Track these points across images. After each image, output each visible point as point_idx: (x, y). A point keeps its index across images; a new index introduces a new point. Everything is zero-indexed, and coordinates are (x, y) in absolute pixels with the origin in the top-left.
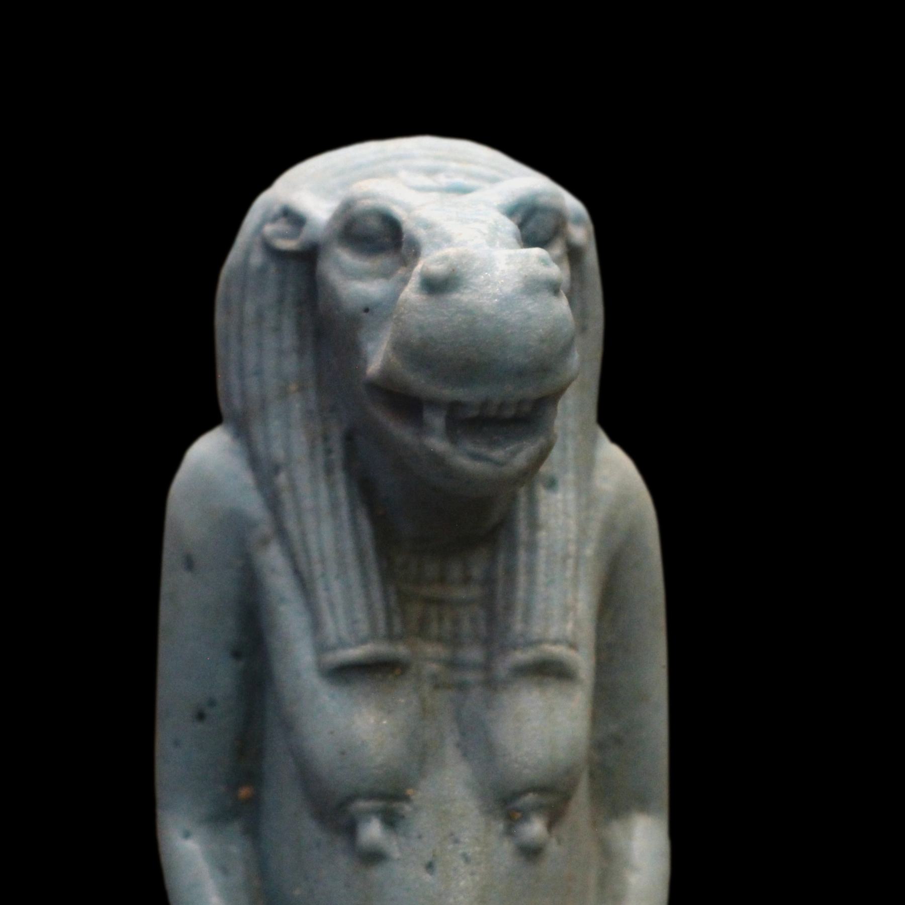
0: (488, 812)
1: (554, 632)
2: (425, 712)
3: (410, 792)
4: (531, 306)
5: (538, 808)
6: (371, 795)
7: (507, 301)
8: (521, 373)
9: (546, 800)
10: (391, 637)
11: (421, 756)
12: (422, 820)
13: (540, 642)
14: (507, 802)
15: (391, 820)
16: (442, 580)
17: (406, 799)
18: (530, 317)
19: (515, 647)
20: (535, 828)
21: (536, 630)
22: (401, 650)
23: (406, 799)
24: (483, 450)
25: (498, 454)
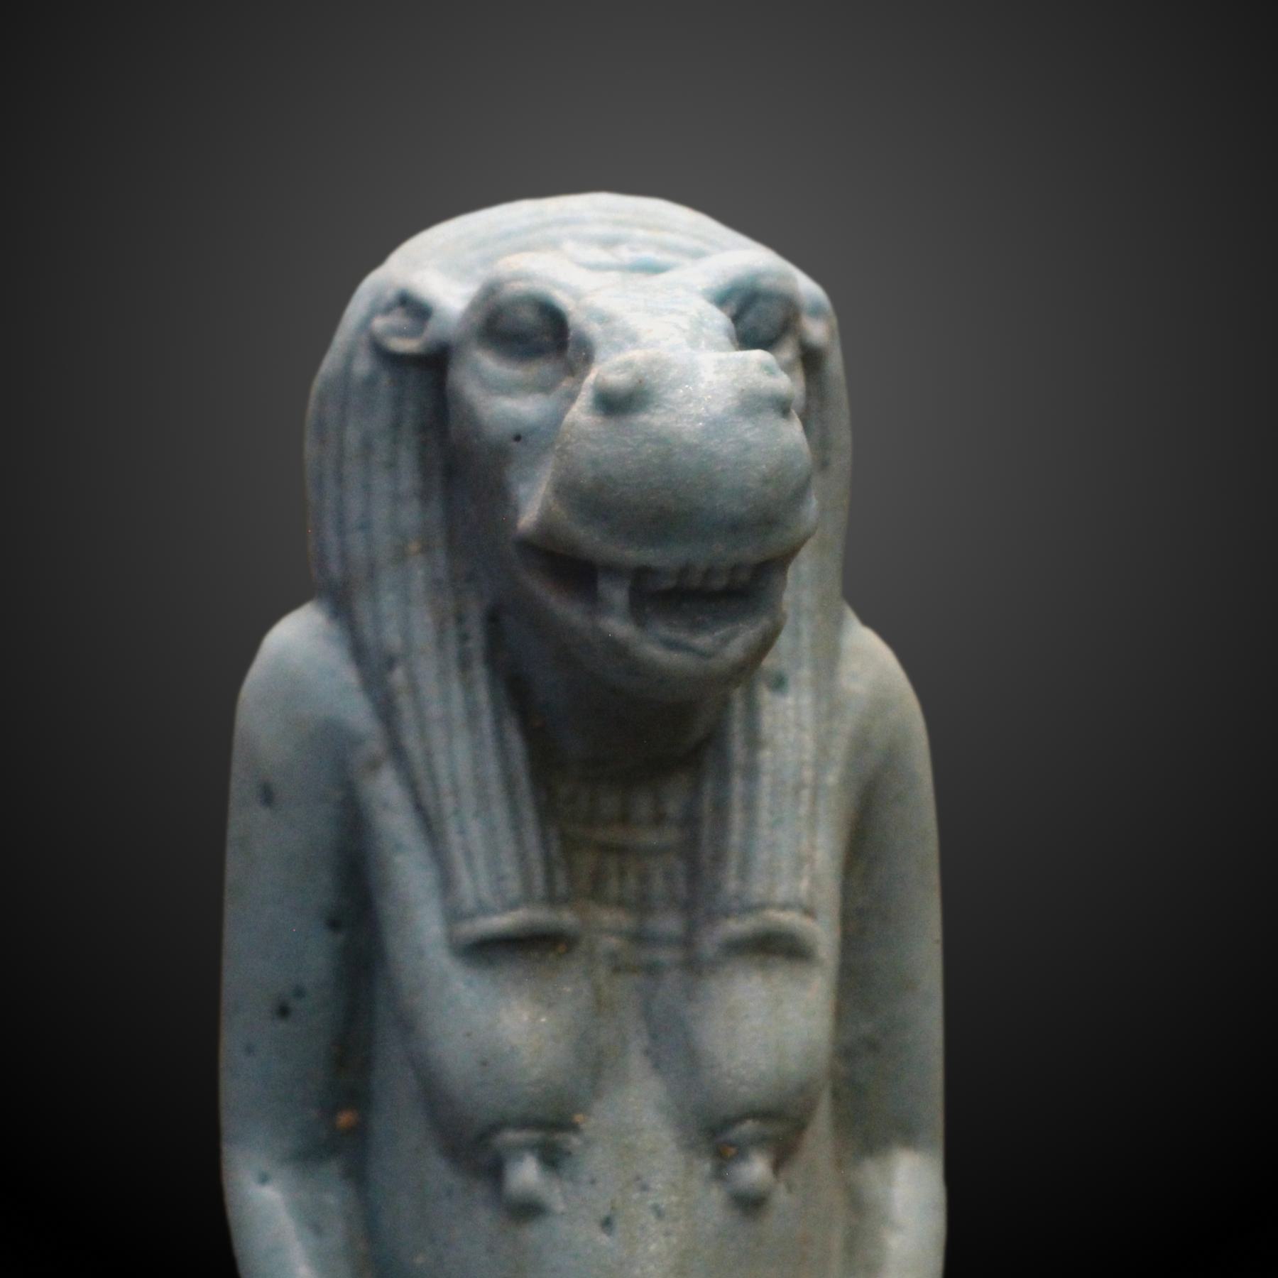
0: (689, 1147)
1: (782, 892)
2: (600, 1006)
3: (578, 1118)
4: (750, 432)
5: (760, 1141)
6: (524, 1123)
7: (716, 425)
8: (735, 527)
9: (771, 1129)
10: (552, 900)
11: (595, 1067)
12: (596, 1158)
13: (762, 906)
14: (716, 1133)
15: (552, 1158)
16: (625, 819)
17: (574, 1128)
18: (748, 448)
19: (727, 914)
20: (756, 1170)
21: (758, 889)
22: (566, 918)
23: (574, 1128)
24: (682, 636)
25: (703, 641)
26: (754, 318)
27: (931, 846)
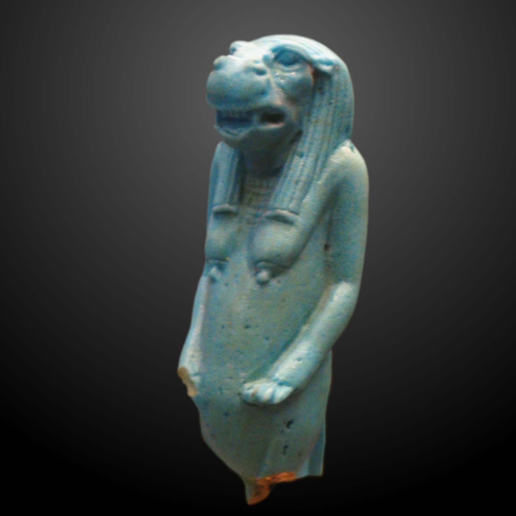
0: (250, 268)
1: (285, 205)
2: (240, 230)
3: (227, 258)
4: (245, 77)
5: (266, 268)
6: (216, 259)
7: (237, 74)
8: (238, 101)
9: (270, 265)
10: (230, 203)
11: (233, 246)
12: (229, 270)
13: (278, 209)
14: (256, 265)
15: (221, 268)
16: (261, 187)
17: (225, 260)
18: (242, 80)
19: (215, 205)
20: (264, 275)
21: (277, 205)
22: (233, 208)
23: (225, 260)
24: (229, 129)
25: (235, 132)
26: (297, 71)
27: (365, 205)
